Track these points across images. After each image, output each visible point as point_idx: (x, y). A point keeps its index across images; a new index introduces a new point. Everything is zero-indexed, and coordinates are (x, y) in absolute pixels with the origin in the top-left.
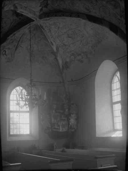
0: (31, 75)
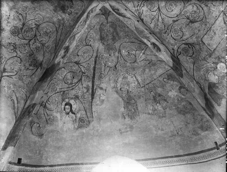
0: (44, 56)
